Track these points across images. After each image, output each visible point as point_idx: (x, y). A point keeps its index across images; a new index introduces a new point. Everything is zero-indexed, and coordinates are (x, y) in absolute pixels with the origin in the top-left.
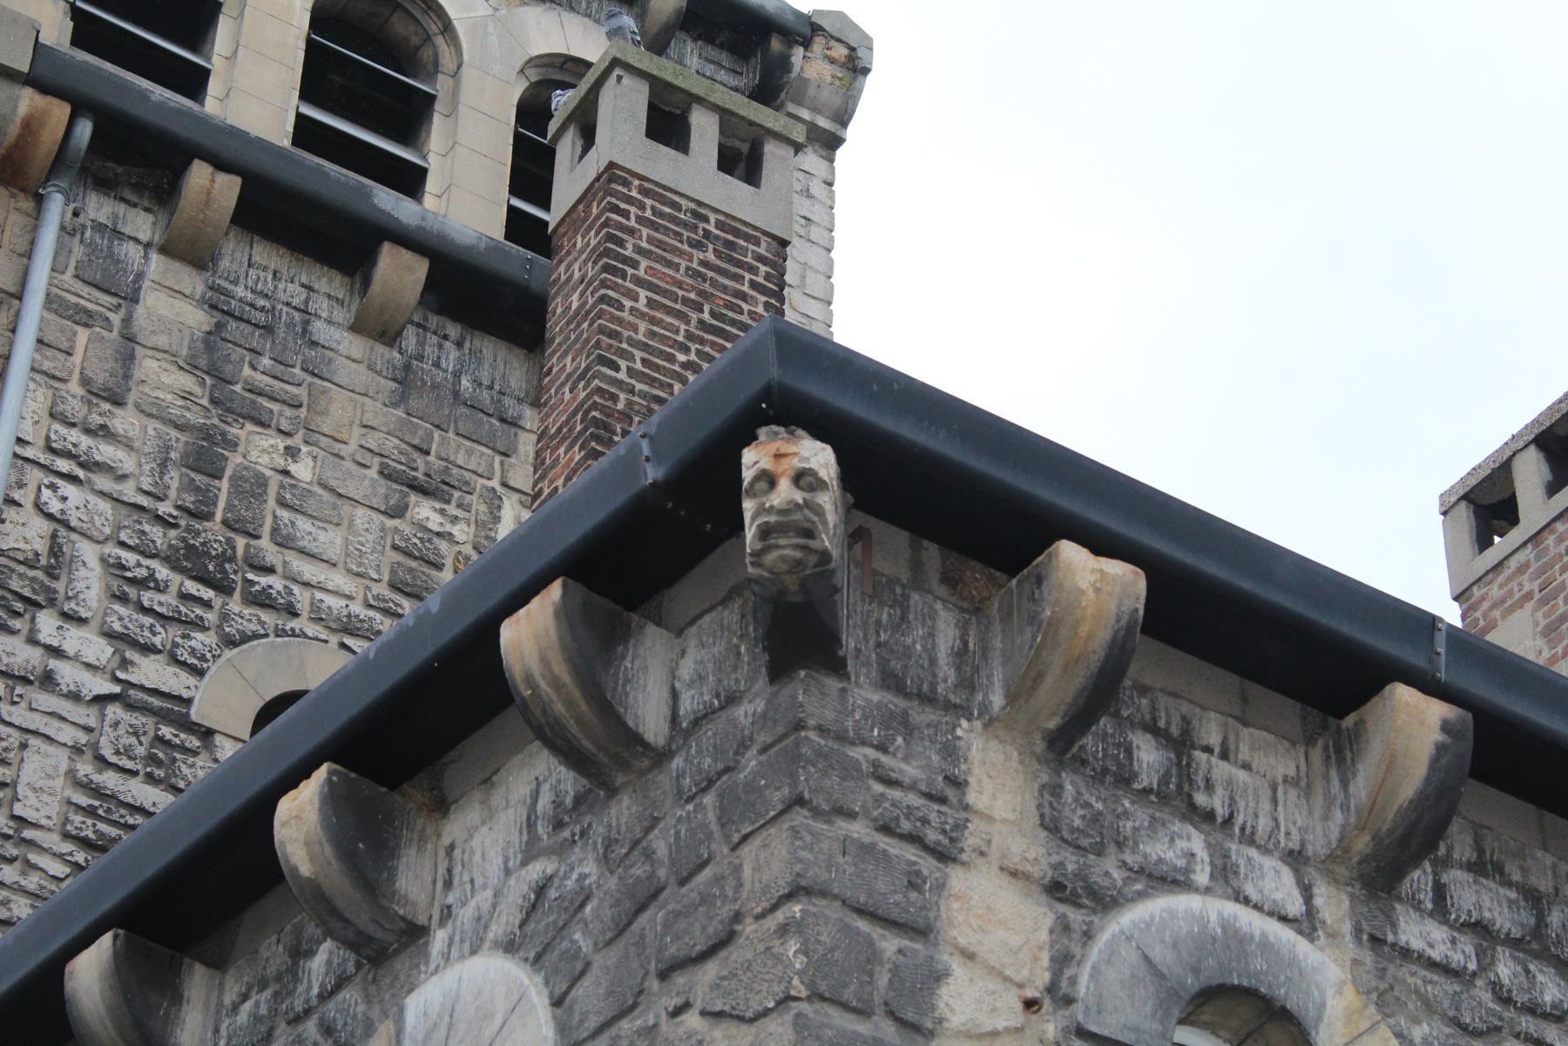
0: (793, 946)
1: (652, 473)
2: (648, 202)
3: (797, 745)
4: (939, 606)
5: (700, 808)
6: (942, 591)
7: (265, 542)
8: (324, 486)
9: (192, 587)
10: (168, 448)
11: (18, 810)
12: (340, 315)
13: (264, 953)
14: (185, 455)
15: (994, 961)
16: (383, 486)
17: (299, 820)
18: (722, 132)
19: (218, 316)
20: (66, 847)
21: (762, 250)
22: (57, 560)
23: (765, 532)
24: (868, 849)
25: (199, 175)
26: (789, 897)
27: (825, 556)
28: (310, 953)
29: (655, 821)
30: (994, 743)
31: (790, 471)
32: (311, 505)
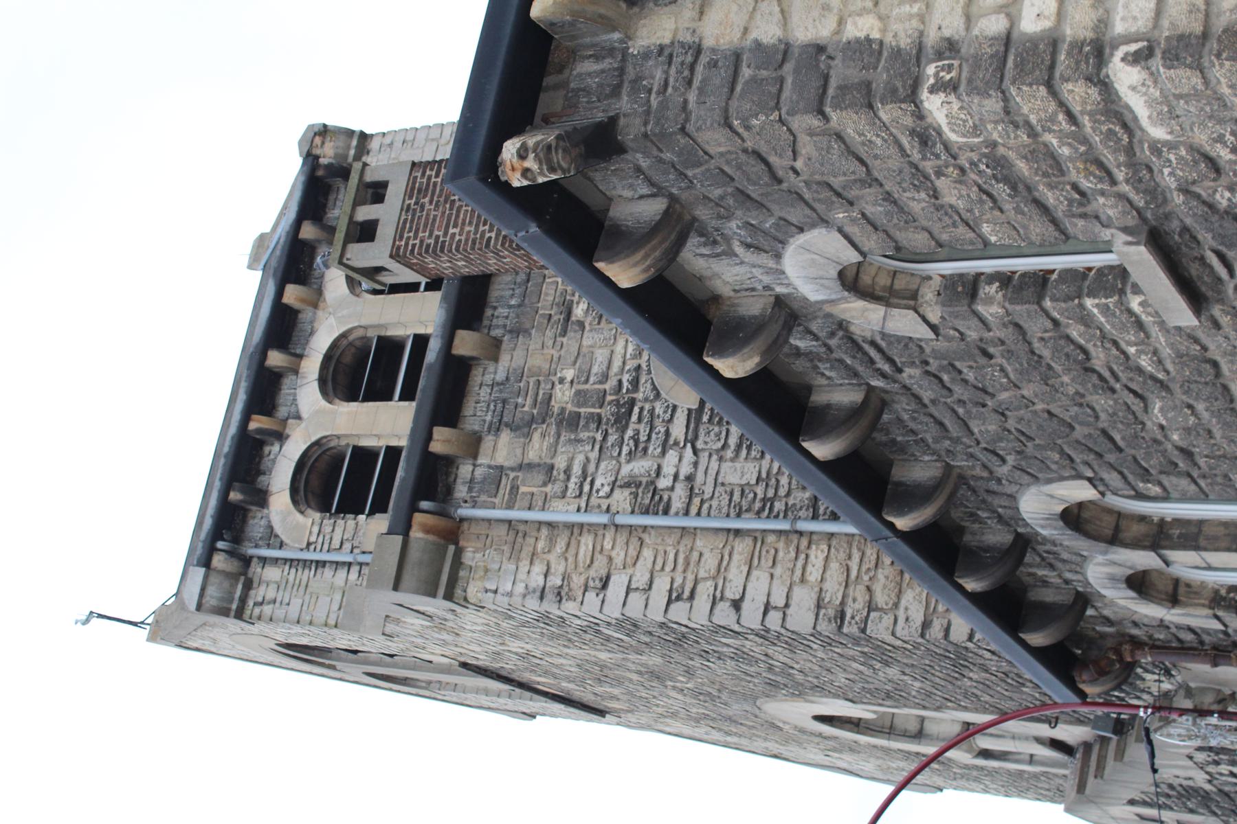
0: (755, 122)
1: (534, 228)
2: (406, 235)
3: (655, 135)
4: (575, 73)
5: (695, 176)
6: (567, 72)
7: (607, 386)
8: (575, 362)
9: (634, 418)
10: (570, 440)
11: (753, 482)
12: (491, 369)
13: (801, 369)
14: (572, 431)
15: (746, 17)
16: (570, 334)
17: (733, 366)
18: (364, 204)
19: (502, 427)
21: (419, 175)
22: (632, 483)
23: (552, 169)
24: (701, 91)
25: (436, 447)
26: (731, 127)
27: (559, 138)
28: (797, 348)
29: (705, 197)
30: (638, 34)
31: (519, 161)
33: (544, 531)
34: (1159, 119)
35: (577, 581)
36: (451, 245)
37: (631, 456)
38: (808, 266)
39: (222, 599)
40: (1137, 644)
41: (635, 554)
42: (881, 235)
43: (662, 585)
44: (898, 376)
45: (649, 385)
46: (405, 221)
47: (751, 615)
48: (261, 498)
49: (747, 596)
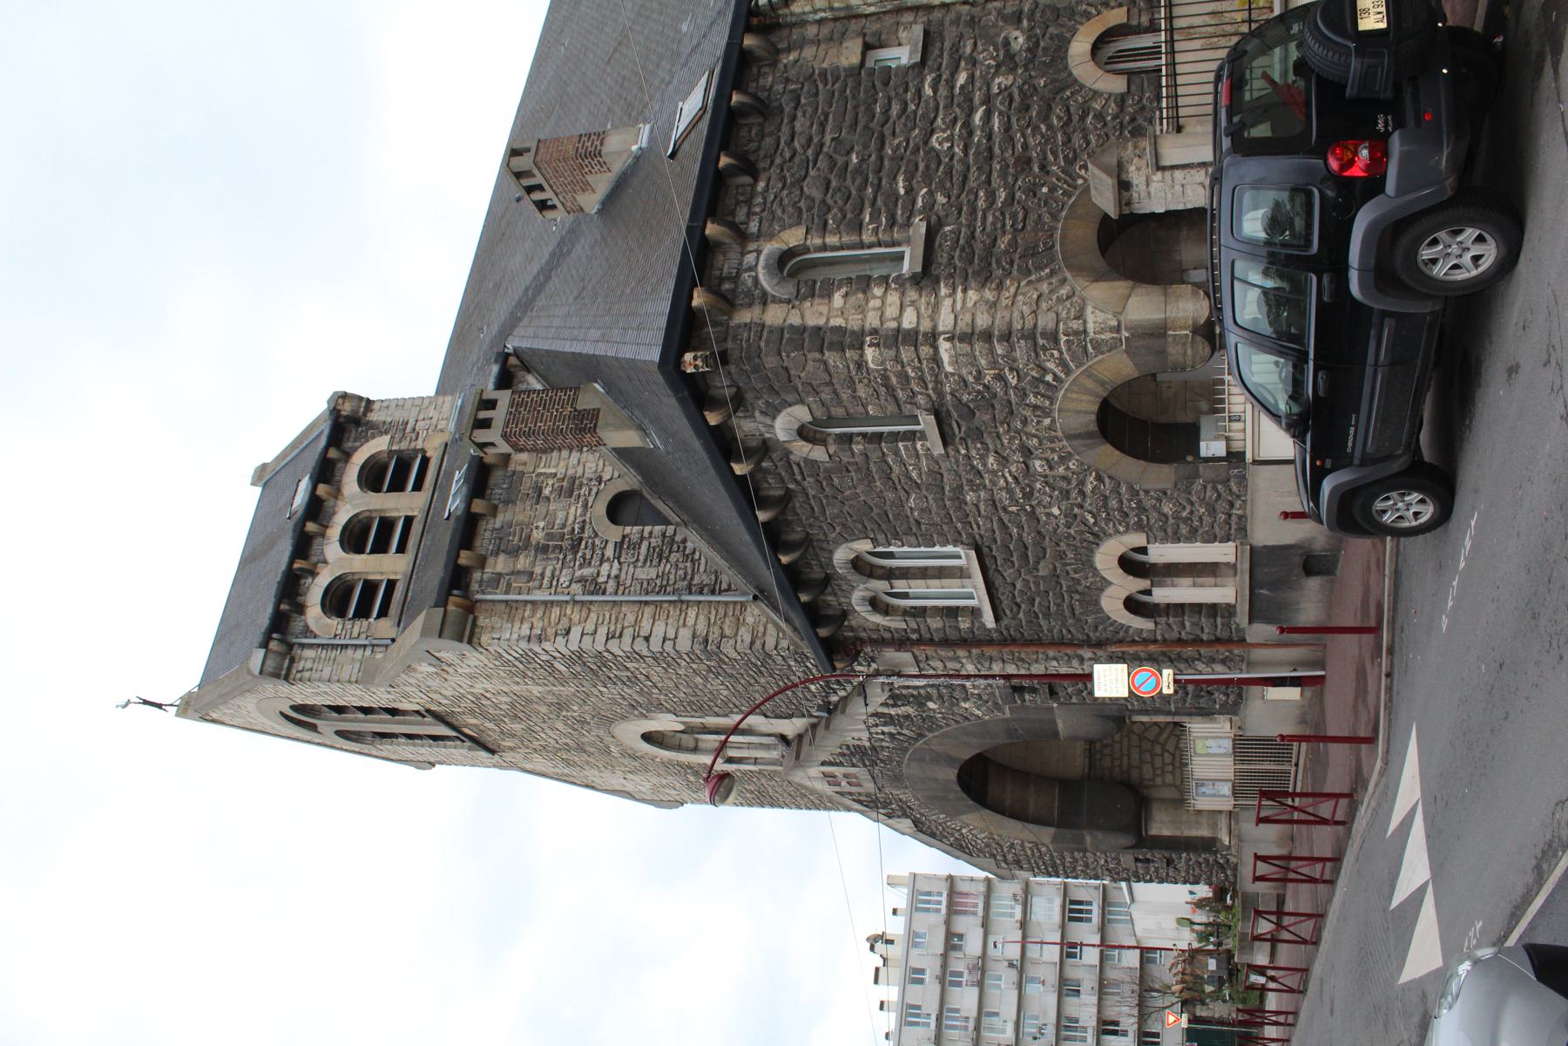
34: (950, 364)
35: (551, 631)
37: (581, 567)
38: (782, 428)
43: (603, 631)
47: (655, 644)
48: (300, 609)
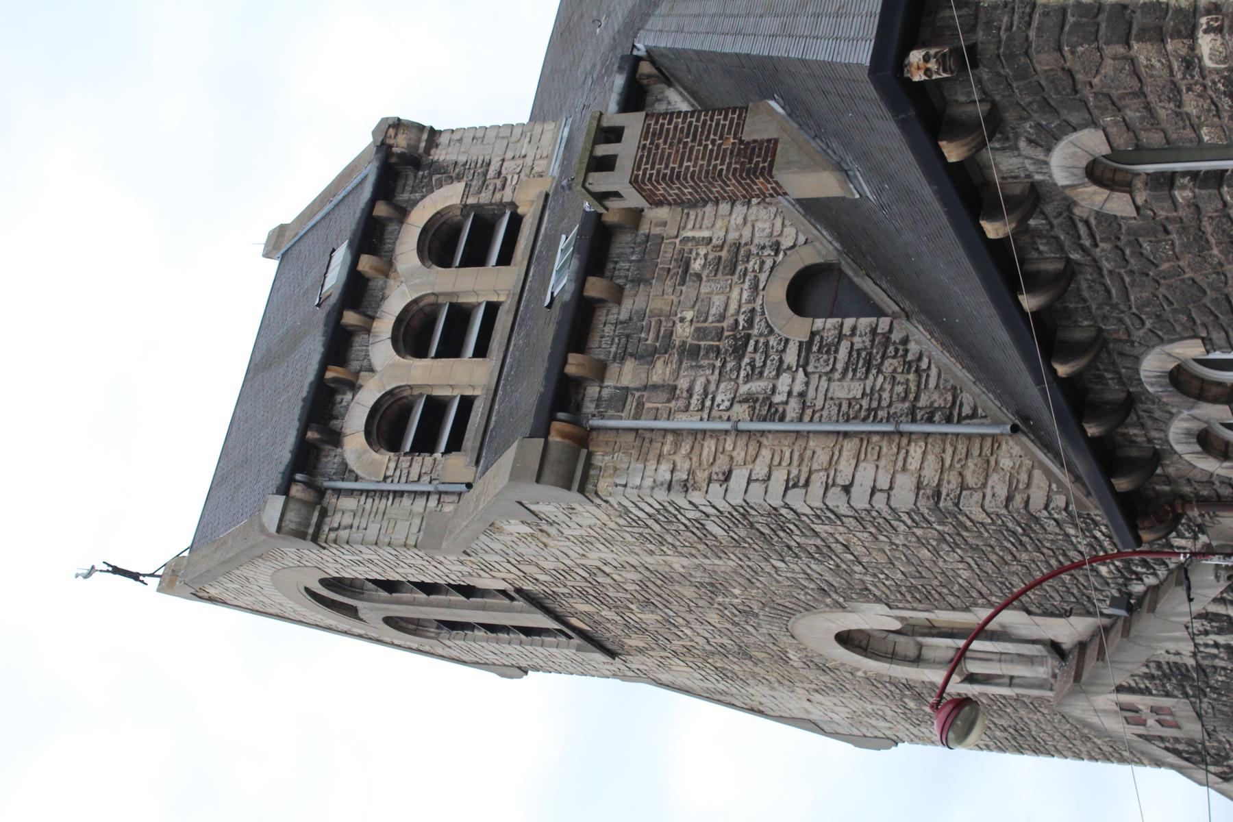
0: (1080, 49)
1: (912, 113)
7: (725, 324)
8: (694, 306)
9: (750, 348)
11: (859, 396)
12: (615, 310)
14: (693, 360)
20: (871, 377)
21: (653, 122)
22: (750, 399)
23: (945, 71)
27: (950, 50)
29: (1018, 103)
32: (704, 309)
33: (670, 438)
36: (686, 174)
37: (748, 378)
38: (1063, 163)
39: (300, 524)
40: (1185, 500)
41: (754, 453)
42: (1131, 134)
43: (779, 476)
44: (1093, 250)
45: (763, 323)
46: (642, 157)
47: (860, 497)
48: (336, 438)
49: (856, 482)
